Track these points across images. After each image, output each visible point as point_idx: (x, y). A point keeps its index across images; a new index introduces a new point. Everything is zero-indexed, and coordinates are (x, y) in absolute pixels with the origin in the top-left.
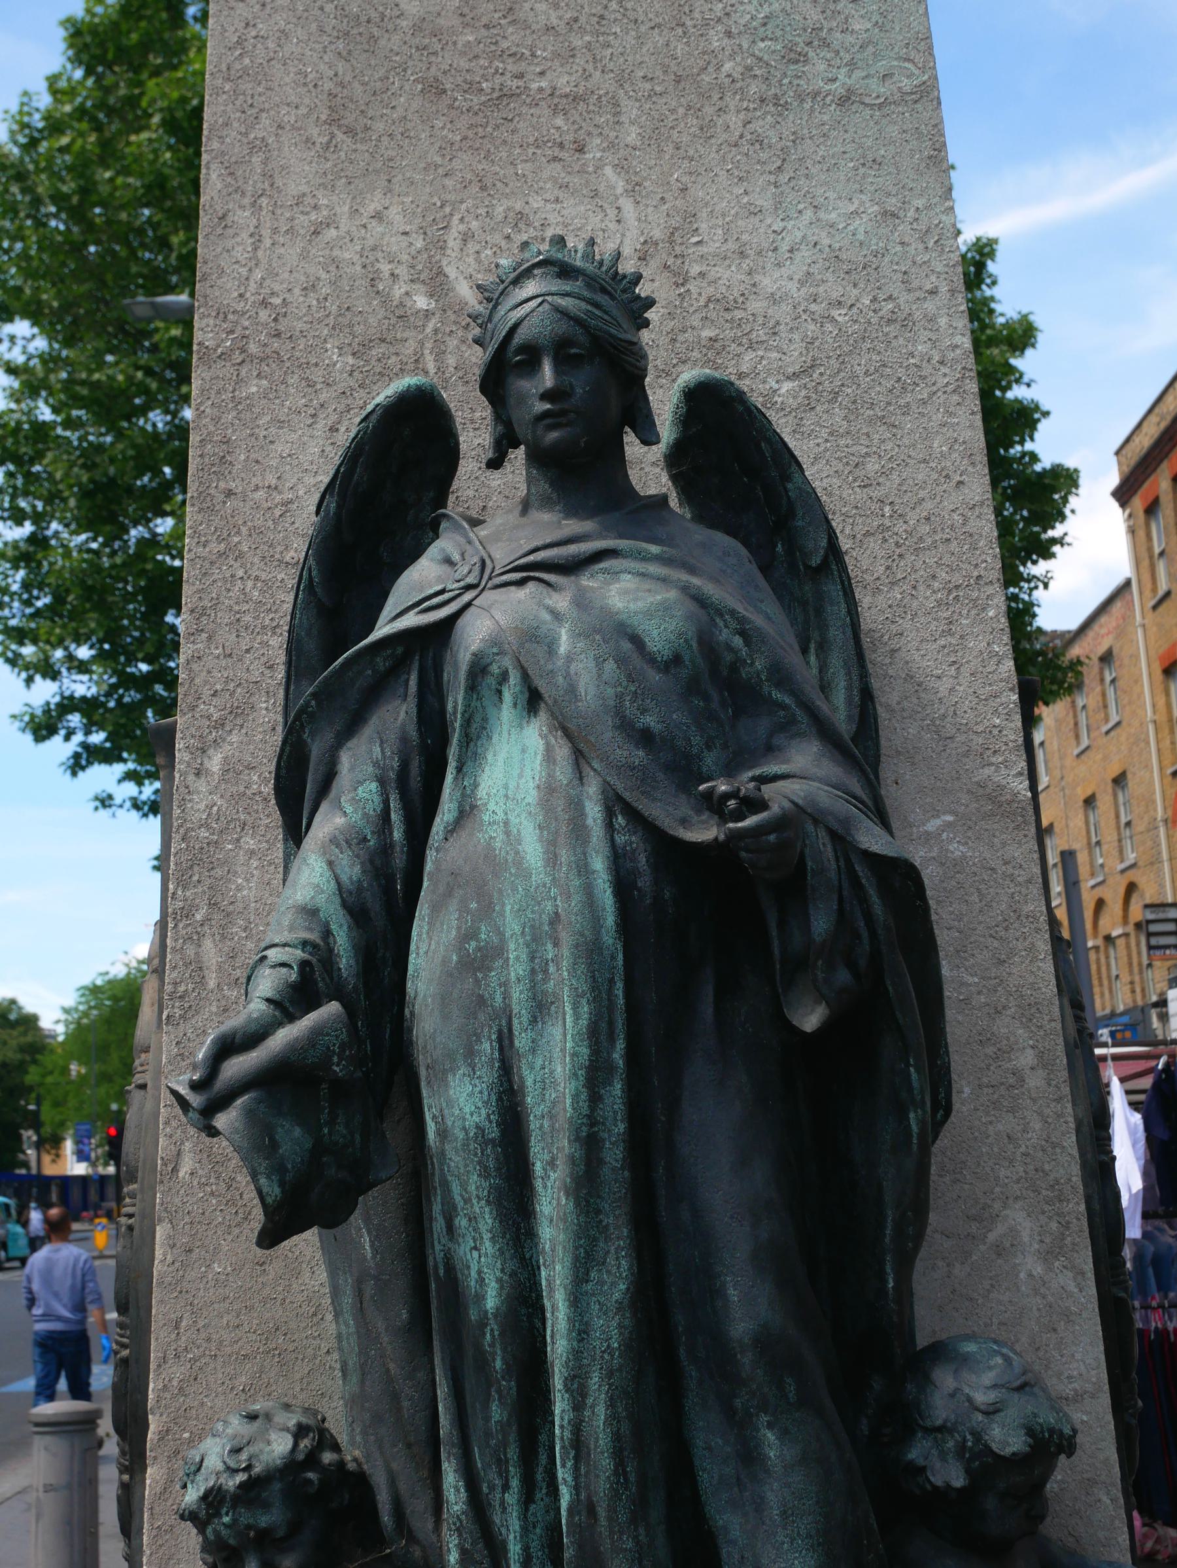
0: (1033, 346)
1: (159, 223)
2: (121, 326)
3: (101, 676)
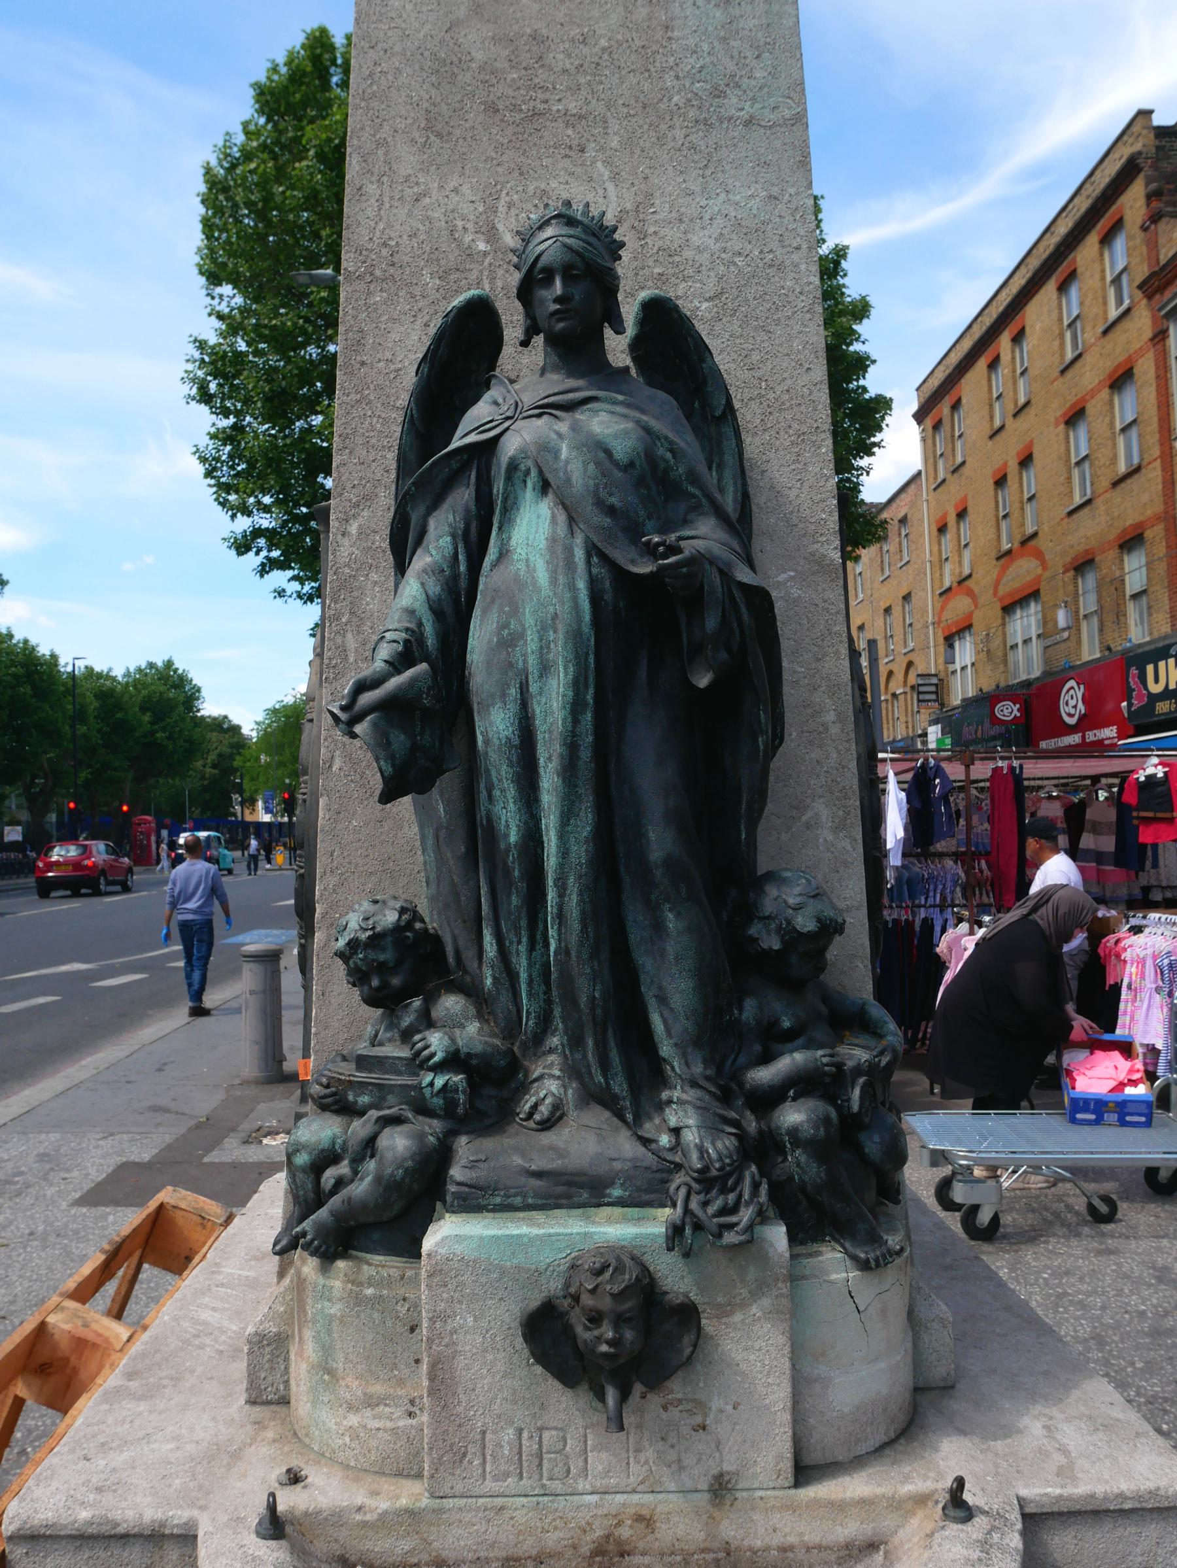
0: (868, 317)
1: (313, 222)
2: (289, 288)
3: (277, 514)
